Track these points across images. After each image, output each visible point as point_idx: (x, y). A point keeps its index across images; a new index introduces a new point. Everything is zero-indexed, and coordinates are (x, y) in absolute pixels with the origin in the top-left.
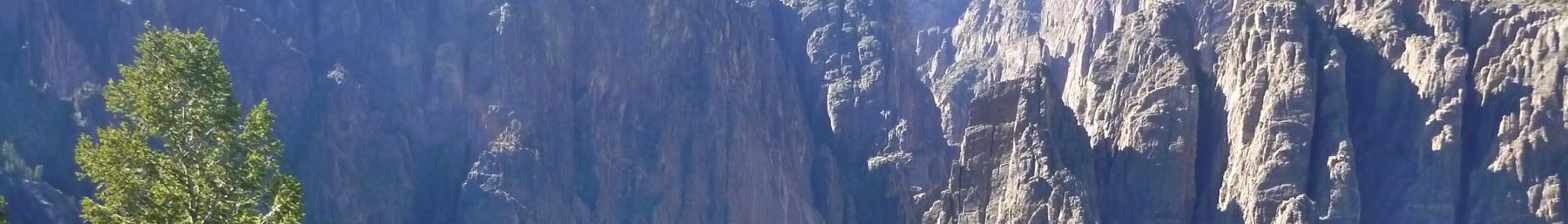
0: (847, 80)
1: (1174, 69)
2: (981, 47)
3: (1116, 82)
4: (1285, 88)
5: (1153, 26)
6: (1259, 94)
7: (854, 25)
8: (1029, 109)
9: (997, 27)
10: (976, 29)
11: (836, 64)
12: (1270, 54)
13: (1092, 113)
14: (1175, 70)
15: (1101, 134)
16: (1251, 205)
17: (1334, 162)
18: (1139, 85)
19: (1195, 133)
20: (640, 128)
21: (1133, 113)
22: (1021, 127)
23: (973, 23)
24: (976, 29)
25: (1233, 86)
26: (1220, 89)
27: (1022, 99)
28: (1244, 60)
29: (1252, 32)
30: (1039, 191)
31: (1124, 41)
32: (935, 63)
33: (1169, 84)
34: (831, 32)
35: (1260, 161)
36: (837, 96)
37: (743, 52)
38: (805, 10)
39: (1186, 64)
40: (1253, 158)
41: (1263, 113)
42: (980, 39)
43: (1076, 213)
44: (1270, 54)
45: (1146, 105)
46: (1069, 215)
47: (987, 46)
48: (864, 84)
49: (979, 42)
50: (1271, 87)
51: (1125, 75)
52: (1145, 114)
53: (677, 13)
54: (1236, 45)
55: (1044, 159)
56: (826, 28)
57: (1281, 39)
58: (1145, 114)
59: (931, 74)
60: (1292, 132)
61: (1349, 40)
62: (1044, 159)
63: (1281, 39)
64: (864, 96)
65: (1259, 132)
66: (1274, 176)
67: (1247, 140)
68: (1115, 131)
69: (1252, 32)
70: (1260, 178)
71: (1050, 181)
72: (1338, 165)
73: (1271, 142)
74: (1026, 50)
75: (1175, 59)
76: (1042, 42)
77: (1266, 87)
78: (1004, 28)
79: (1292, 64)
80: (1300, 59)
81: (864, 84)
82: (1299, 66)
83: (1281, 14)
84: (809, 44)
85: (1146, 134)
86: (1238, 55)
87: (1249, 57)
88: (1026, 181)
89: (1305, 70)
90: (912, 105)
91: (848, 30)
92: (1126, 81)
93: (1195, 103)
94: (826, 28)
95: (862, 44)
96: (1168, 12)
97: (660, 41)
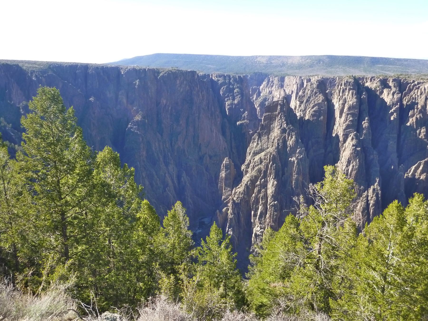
0: (231, 101)
1: (320, 98)
2: (268, 92)
3: (305, 101)
4: (351, 103)
5: (315, 86)
6: (344, 105)
8: (281, 109)
9: (272, 86)
12: (347, 94)
13: (298, 110)
14: (321, 98)
15: (301, 115)
16: (342, 135)
17: (364, 123)
18: (311, 102)
21: (309, 110)
23: (266, 85)
24: (267, 87)
25: (337, 102)
26: (333, 103)
27: (279, 106)
28: (340, 95)
30: (284, 131)
31: (307, 90)
32: (255, 96)
34: (227, 88)
37: (203, 93)
38: (220, 82)
39: (324, 96)
40: (342, 122)
41: (345, 110)
42: (268, 89)
43: (294, 137)
44: (347, 94)
45: (313, 108)
46: (292, 137)
47: (270, 91)
48: (236, 102)
49: (267, 90)
50: (347, 103)
51: (307, 99)
52: (313, 110)
53: (185, 82)
54: (337, 91)
55: (285, 122)
57: (350, 90)
58: (313, 110)
59: (254, 99)
60: (353, 115)
62: (285, 122)
63: (350, 90)
64: (236, 105)
65: (344, 115)
66: (348, 127)
67: (340, 117)
68: (304, 114)
70: (344, 127)
71: (287, 128)
72: (365, 124)
73: (347, 118)
74: (280, 92)
75: (321, 95)
76: (284, 90)
77: (346, 103)
78: (274, 87)
79: (353, 96)
81: (236, 102)
83: (350, 83)
85: (313, 115)
86: (338, 94)
87: (341, 94)
88: (280, 128)
89: (356, 98)
90: (249, 108)
92: (307, 101)
93: (326, 107)
95: (235, 91)
97: (180, 90)
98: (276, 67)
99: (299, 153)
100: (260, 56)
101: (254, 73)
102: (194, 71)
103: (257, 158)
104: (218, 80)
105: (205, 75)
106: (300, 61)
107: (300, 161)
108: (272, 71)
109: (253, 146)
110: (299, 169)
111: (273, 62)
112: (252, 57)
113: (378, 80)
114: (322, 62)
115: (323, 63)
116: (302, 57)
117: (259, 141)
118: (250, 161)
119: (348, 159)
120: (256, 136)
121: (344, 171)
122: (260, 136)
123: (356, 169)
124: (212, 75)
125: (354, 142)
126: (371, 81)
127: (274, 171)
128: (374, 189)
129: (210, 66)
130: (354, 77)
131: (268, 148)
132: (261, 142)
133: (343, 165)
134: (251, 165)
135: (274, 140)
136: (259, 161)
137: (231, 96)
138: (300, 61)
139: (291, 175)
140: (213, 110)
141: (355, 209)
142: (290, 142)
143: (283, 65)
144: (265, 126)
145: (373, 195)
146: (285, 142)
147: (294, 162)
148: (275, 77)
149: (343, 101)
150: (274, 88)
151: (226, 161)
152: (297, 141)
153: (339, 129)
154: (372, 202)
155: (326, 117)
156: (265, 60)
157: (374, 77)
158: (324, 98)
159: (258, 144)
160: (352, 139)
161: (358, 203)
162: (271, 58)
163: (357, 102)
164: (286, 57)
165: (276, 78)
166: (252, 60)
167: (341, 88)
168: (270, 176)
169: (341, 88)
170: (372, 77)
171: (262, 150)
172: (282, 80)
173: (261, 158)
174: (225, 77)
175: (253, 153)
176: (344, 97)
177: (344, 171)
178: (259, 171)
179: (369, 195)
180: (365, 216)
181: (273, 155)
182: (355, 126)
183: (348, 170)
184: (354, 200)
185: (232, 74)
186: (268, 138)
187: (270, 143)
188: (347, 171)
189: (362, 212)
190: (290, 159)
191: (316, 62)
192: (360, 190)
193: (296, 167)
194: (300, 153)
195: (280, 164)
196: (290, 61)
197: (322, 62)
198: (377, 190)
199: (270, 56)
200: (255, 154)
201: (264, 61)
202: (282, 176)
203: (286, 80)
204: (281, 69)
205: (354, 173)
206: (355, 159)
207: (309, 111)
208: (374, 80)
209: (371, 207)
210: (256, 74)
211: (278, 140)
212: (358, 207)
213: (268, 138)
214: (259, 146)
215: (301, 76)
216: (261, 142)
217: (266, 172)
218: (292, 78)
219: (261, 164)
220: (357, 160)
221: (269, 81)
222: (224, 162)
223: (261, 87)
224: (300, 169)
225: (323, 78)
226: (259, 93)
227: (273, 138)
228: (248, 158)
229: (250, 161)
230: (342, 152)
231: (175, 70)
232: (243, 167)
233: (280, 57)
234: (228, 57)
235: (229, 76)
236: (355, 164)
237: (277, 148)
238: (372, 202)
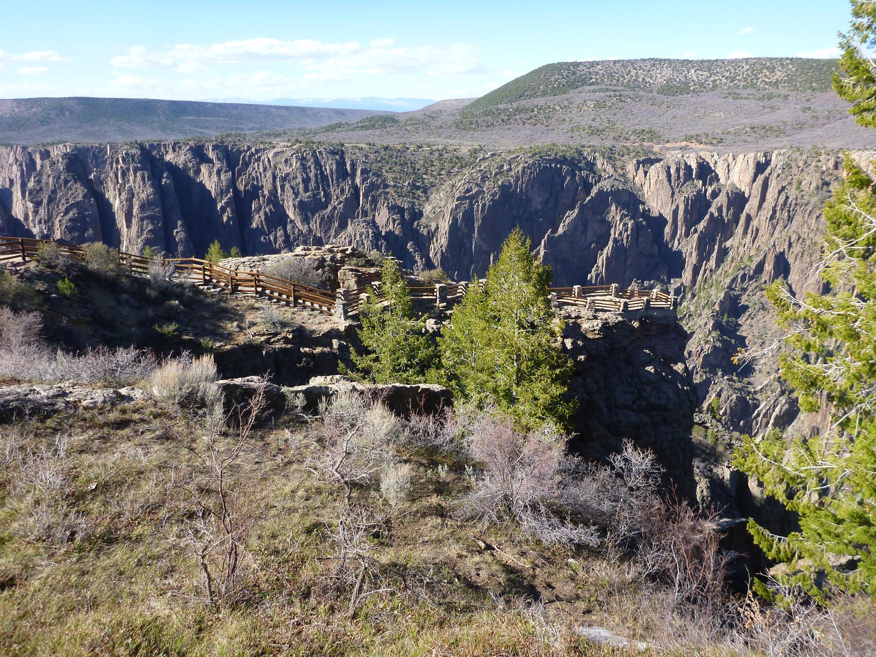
1: (79, 192)
3: (45, 201)
4: (143, 196)
6: (130, 200)
12: (131, 178)
14: (79, 191)
17: (177, 232)
25: (115, 198)
28: (118, 183)
31: (44, 177)
33: (78, 199)
35: (138, 237)
39: (85, 187)
41: (135, 210)
44: (131, 178)
45: (66, 212)
51: (50, 196)
61: (171, 168)
63: (136, 170)
65: (135, 221)
73: (142, 226)
77: (133, 196)
79: (144, 183)
83: (133, 156)
85: (70, 230)
86: (114, 180)
87: (120, 181)
89: (153, 185)
92: (51, 200)
93: (95, 209)
96: (69, 158)
106: (16, 110)
116: (19, 102)
126: (174, 150)
130: (139, 145)
138: (16, 110)
155: (99, 229)
158: (86, 190)
191: (54, 112)
207: (60, 221)
208: (180, 148)
225: (76, 147)
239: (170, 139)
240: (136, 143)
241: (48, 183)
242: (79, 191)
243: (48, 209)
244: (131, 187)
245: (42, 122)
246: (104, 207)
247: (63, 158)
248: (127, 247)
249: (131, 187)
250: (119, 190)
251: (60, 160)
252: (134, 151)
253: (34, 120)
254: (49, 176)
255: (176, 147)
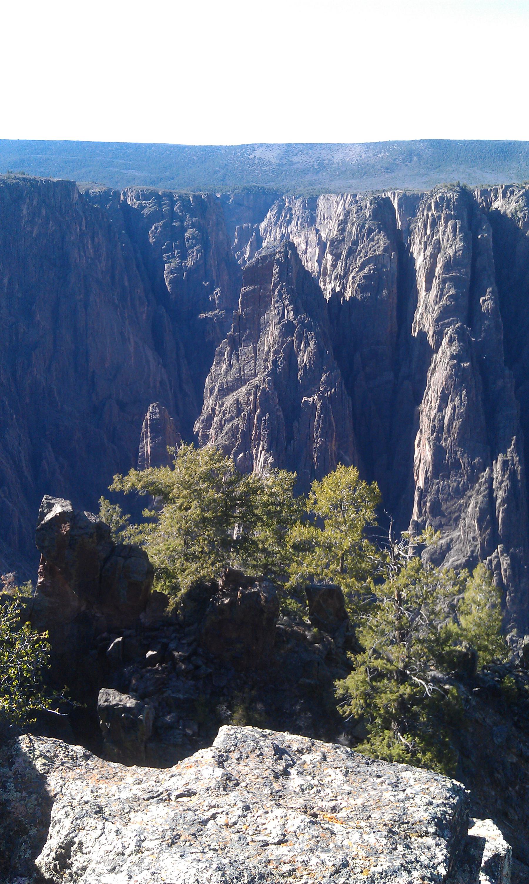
0: (178, 260)
1: (381, 241)
2: (279, 236)
3: (344, 254)
4: (450, 252)
5: (367, 213)
6: (434, 257)
7: (182, 222)
8: (280, 273)
9: (289, 222)
10: (276, 224)
11: (169, 249)
12: (441, 229)
13: (330, 276)
14: (381, 243)
15: (333, 289)
16: (431, 334)
17: (484, 301)
18: (359, 254)
19: (395, 286)
20: (20, 295)
21: (353, 274)
22: (275, 286)
23: (273, 220)
24: (276, 224)
25: (419, 252)
26: (412, 254)
27: (275, 266)
28: (426, 234)
29: (430, 214)
30: (287, 329)
31: (349, 225)
32: (248, 249)
33: (377, 253)
34: (164, 226)
35: (436, 303)
36: (171, 272)
37: (96, 240)
38: (146, 211)
39: (388, 239)
40: (432, 301)
41: (437, 270)
42: (278, 231)
43: (312, 343)
44: (441, 229)
45: (361, 268)
46: (307, 345)
47: (283, 235)
48: (190, 263)
49: (278, 233)
50: (442, 252)
51: (350, 248)
52: (361, 274)
53: (44, 211)
54: (420, 224)
55: (290, 307)
56: (161, 223)
57: (448, 218)
58: (361, 274)
59: (246, 256)
60: (456, 282)
61: (498, 217)
62: (290, 307)
63: (448, 218)
64: (190, 272)
65: (435, 283)
66: (445, 313)
67: (428, 289)
68: (344, 288)
69: (430, 214)
70: (436, 314)
71: (295, 322)
72: (486, 302)
73: (442, 289)
74: (307, 237)
75: (381, 236)
76: (317, 231)
77: (439, 252)
78: (294, 223)
79: (455, 235)
80: (460, 231)
81: (190, 263)
82: (459, 236)
83: (449, 201)
84: (150, 235)
85: (362, 288)
86: (422, 231)
87: (428, 232)
88: (279, 323)
89: (463, 239)
90: (226, 278)
91: (177, 224)
92: (351, 252)
93: (395, 265)
94: (161, 223)
95: (187, 235)
96: (378, 203)
97: (32, 232)
98: (305, 172)
99: (325, 382)
100: (261, 145)
101: (245, 188)
102: (69, 182)
103: (229, 401)
104: (142, 207)
105: (106, 193)
106: (364, 155)
107: (329, 403)
108: (293, 183)
109: (220, 371)
110: (326, 422)
111: (295, 159)
112: (241, 147)
113: (521, 193)
114: (415, 159)
115: (419, 160)
116: (368, 146)
117: (234, 357)
118: (213, 410)
119: (443, 392)
120: (224, 346)
121: (434, 421)
122: (235, 345)
123: (461, 415)
124: (125, 194)
125: (455, 348)
126: (504, 196)
127: (266, 431)
128: (505, 463)
129: (132, 172)
130: (461, 188)
131: (256, 375)
132: (238, 360)
133: (430, 409)
134: (215, 419)
135: (268, 353)
136: (233, 409)
137: (176, 247)
138: (364, 155)
139: (310, 438)
140: (126, 284)
141: (463, 515)
142: (304, 358)
143: (322, 167)
144: (246, 319)
145: (503, 475)
146: (291, 356)
147: (314, 405)
148: (296, 198)
149: (433, 248)
150: (292, 227)
151: (151, 413)
152: (319, 354)
153: (425, 318)
154: (500, 495)
155: (395, 290)
156: (275, 154)
157: (512, 186)
158: (388, 242)
159: (230, 366)
160: (451, 341)
161: (470, 497)
162: (290, 149)
163: (464, 249)
164: (328, 147)
165: (298, 202)
166: (242, 155)
167: (427, 215)
168: (259, 445)
169: (427, 215)
170: (507, 187)
171: (240, 381)
172: (311, 205)
173: (237, 400)
174: (159, 198)
175: (219, 390)
176: (435, 238)
177: (434, 421)
178: (234, 432)
179: (495, 476)
180: (486, 529)
181: (263, 391)
182: (461, 310)
183: (443, 417)
184: (460, 493)
185: (178, 191)
186: (255, 350)
187: (260, 363)
188: (439, 420)
189: (480, 521)
190: (305, 399)
191: (401, 158)
192: (473, 467)
193: (319, 417)
194: (329, 383)
195: (280, 413)
196: (338, 157)
197: (415, 159)
198: (513, 464)
199: (288, 145)
200: (225, 391)
201: (272, 157)
202: (289, 441)
203: (320, 205)
204: (315, 177)
205: (457, 424)
206: (458, 388)
207: (353, 277)
208: (512, 193)
209: (499, 506)
210: (248, 191)
211: (276, 353)
212: (470, 509)
213: (255, 350)
214: (233, 370)
215: (355, 192)
216: (238, 360)
217: (246, 435)
218: (334, 198)
219: (238, 415)
220: (464, 393)
221: (281, 208)
222: (148, 416)
223: (263, 225)
224: (330, 424)
225: (405, 195)
226: (259, 240)
227: (266, 348)
228: (209, 402)
229: (213, 410)
230: (429, 374)
231: (15, 178)
232: (198, 426)
233: (311, 146)
234: (180, 149)
235: (170, 196)
236: (457, 402)
237: (273, 373)
238: (500, 495)
239: (502, 182)
240: (458, 185)
241: (351, 232)
242: (381, 243)
243: (346, 263)
244: (438, 240)
245: (387, 169)
246: (406, 263)
247: (371, 204)
248: (422, 314)
249: (438, 240)
250: (425, 243)
251: (368, 205)
252: (450, 195)
253: (379, 167)
254: (353, 225)
255: (508, 191)
